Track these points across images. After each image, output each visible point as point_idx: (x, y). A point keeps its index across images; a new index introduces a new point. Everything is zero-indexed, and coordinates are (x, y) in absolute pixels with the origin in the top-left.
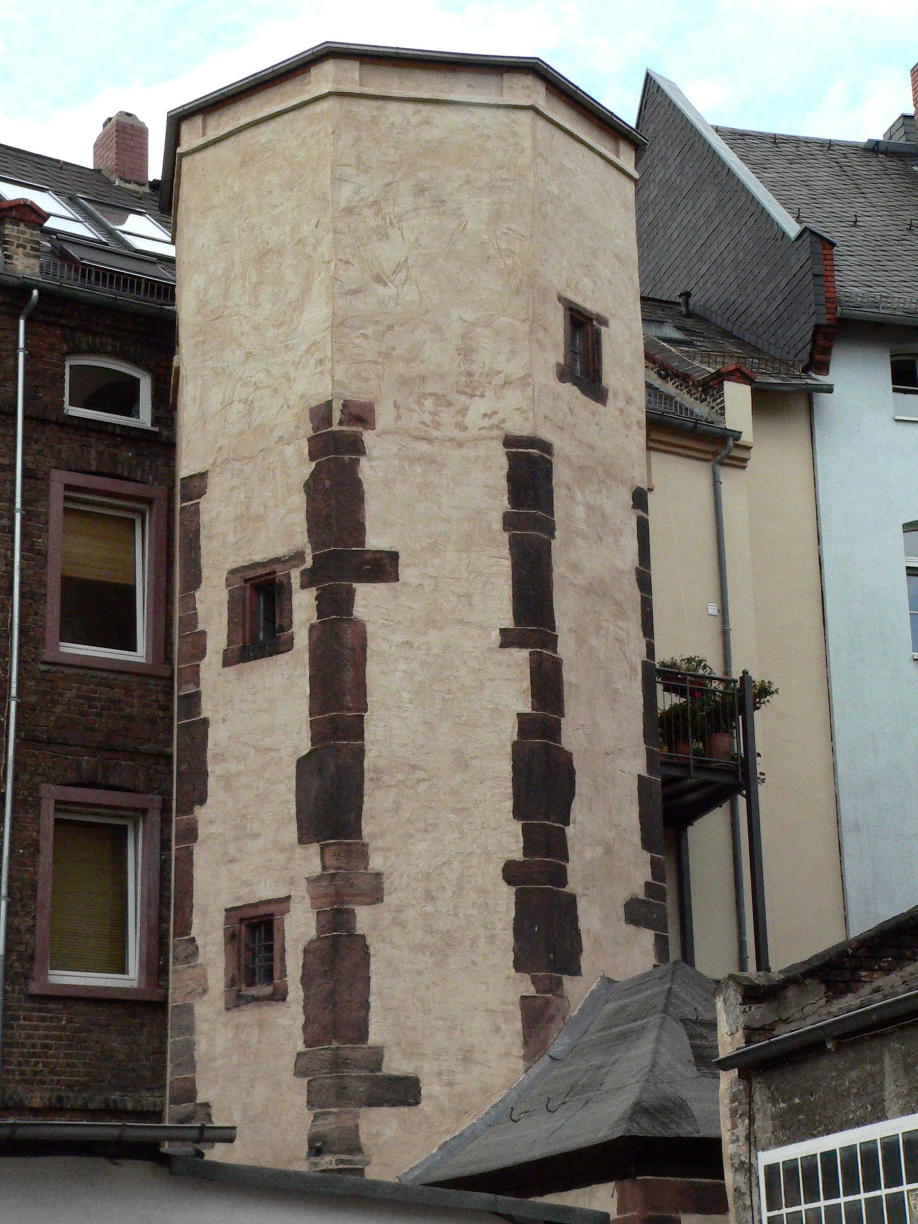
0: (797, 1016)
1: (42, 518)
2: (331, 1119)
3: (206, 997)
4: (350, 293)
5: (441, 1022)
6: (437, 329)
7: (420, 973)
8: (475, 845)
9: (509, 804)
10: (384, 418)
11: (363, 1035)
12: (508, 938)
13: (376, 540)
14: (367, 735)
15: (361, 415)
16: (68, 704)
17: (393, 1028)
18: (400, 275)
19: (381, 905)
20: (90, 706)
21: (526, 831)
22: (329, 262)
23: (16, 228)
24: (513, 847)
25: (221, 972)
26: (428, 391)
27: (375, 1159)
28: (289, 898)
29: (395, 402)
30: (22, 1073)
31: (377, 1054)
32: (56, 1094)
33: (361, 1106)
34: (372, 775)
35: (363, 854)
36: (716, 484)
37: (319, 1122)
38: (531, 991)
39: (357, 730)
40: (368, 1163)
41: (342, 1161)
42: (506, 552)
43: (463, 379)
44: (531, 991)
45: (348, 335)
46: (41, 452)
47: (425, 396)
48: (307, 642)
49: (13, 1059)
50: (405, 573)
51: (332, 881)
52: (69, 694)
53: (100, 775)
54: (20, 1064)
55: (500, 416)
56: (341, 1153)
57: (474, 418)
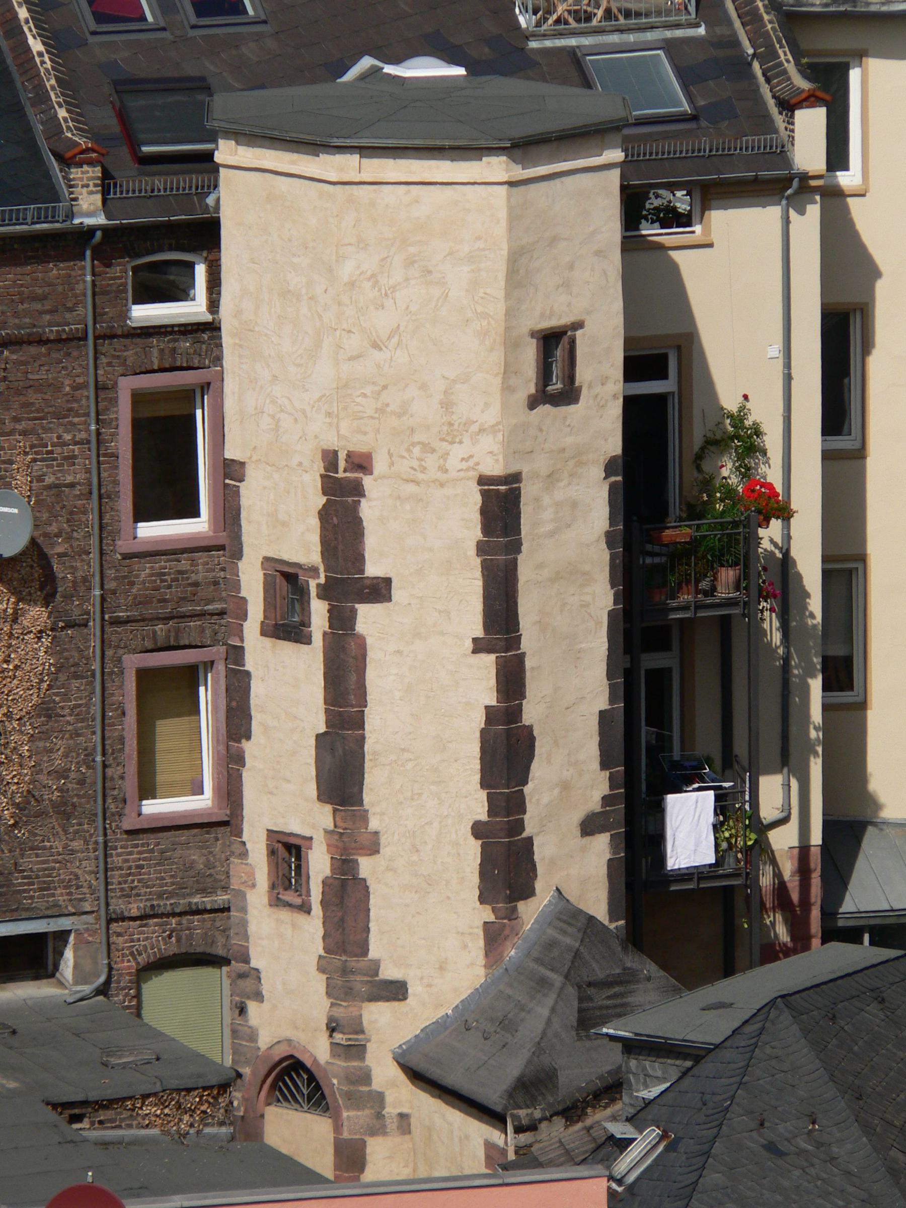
0: (546, 1139)
1: (114, 423)
2: (341, 1010)
3: (254, 890)
4: (351, 359)
5: (423, 941)
6: (424, 387)
7: (407, 905)
8: (450, 810)
9: (477, 777)
10: (380, 465)
11: (365, 951)
12: (475, 879)
13: (373, 569)
14: (366, 726)
15: (361, 463)
16: (144, 582)
17: (388, 946)
18: (393, 340)
19: (378, 856)
20: (162, 581)
21: (491, 799)
22: (335, 330)
23: (79, 170)
24: (480, 810)
25: (265, 876)
26: (416, 440)
27: (373, 1038)
28: (311, 838)
29: (389, 450)
30: (122, 890)
31: (375, 966)
32: (148, 904)
33: (363, 1002)
34: (371, 757)
35: (364, 818)
36: (786, 221)
37: (334, 1009)
38: (491, 918)
39: (359, 722)
40: (369, 1041)
41: (350, 1039)
42: (478, 573)
43: (445, 428)
44: (491, 918)
45: (351, 395)
46: (109, 364)
47: (413, 444)
48: (321, 644)
49: (114, 881)
50: (396, 593)
51: (340, 837)
52: (143, 575)
53: (172, 639)
54: (120, 883)
55: (475, 459)
56: (350, 1034)
57: (453, 463)
